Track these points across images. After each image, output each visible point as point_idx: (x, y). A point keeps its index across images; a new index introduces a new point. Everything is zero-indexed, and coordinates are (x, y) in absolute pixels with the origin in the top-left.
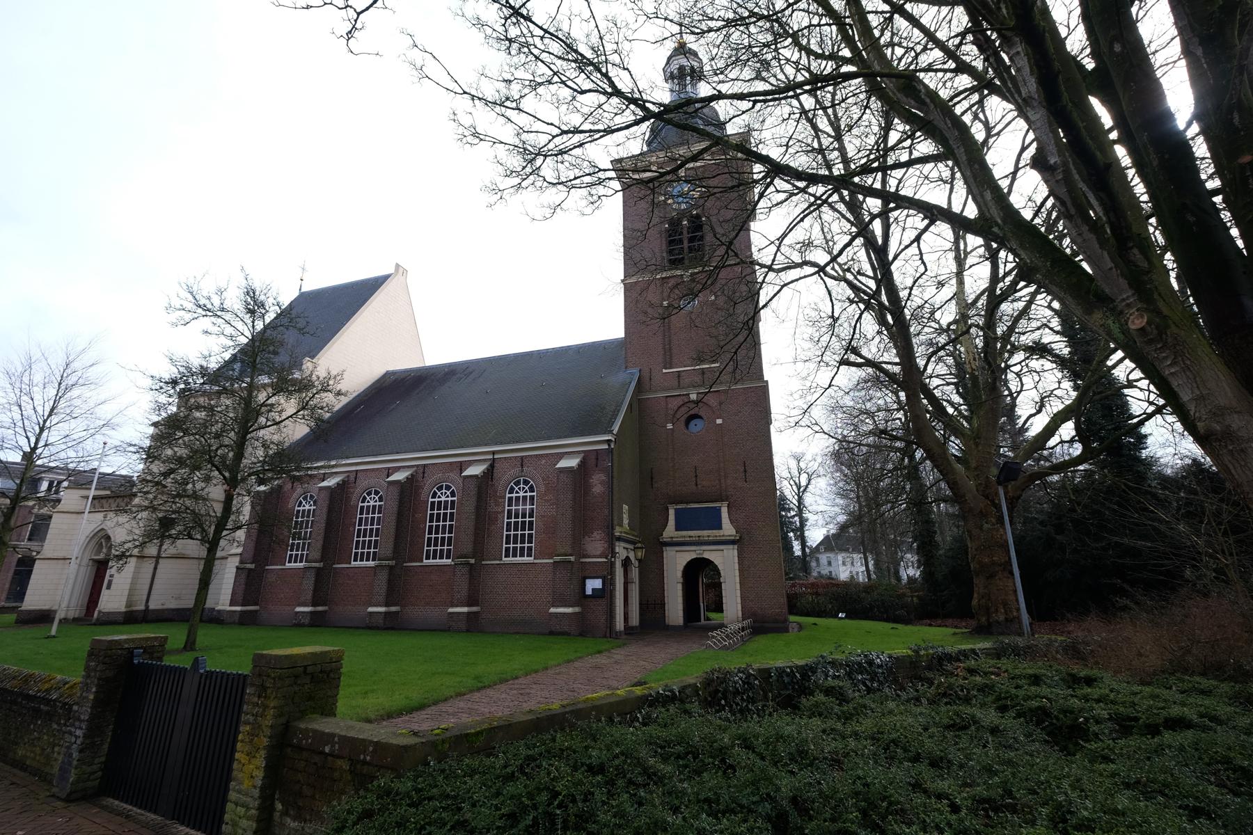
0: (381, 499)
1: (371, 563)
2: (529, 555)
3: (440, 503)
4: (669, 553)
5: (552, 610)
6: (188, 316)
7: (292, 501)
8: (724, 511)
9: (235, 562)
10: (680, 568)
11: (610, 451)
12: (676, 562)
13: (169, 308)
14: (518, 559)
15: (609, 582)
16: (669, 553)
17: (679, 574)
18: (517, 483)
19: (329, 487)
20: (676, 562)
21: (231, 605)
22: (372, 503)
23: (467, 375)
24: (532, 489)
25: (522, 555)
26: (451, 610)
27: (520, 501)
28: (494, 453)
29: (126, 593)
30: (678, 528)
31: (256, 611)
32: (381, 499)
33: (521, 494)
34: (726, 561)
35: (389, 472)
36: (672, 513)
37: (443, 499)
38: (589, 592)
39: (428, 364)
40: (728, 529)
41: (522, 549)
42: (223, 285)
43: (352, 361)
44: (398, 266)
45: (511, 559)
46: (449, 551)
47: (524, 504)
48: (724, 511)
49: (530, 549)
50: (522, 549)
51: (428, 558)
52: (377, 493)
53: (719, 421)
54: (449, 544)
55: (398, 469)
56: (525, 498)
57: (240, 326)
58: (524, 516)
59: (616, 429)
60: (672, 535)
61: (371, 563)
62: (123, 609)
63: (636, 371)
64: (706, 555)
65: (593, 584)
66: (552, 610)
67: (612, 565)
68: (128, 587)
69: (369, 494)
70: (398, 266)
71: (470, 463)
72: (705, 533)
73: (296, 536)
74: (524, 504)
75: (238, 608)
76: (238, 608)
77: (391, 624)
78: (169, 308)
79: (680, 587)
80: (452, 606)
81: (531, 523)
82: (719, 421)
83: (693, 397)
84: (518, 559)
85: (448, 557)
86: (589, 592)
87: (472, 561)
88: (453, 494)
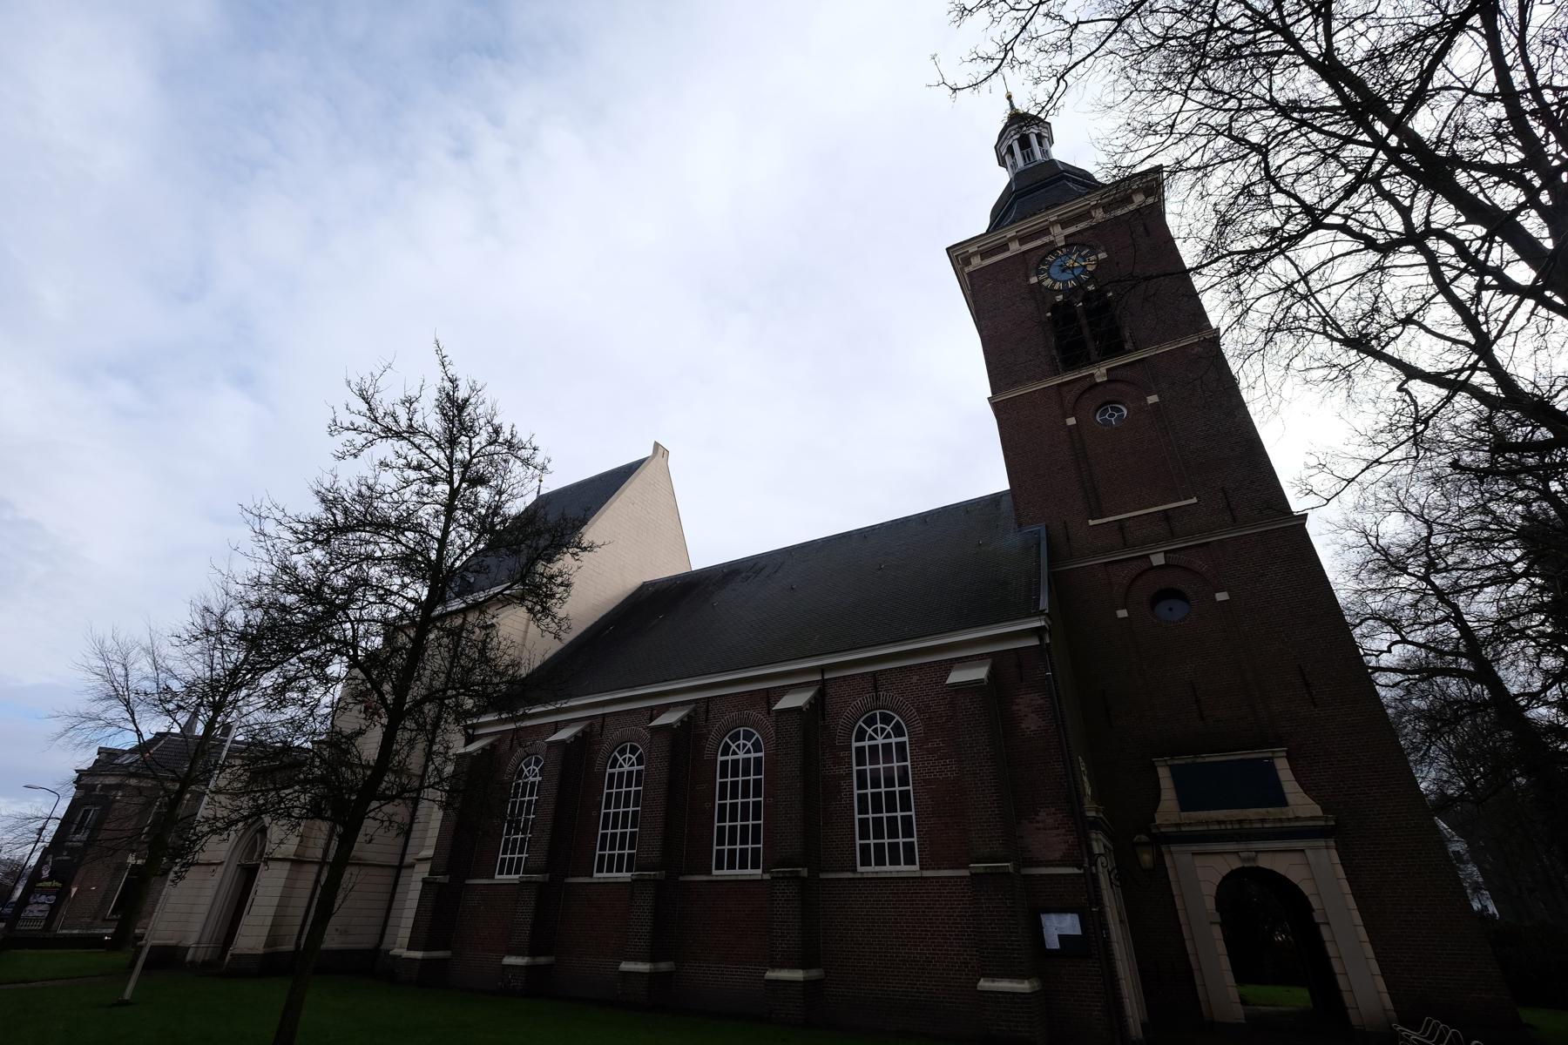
0: (640, 761)
1: (625, 876)
2: (910, 861)
3: (735, 762)
4: (1179, 859)
5: (984, 984)
6: (360, 440)
7: (510, 768)
8: (1283, 767)
9: (423, 871)
10: (1209, 890)
11: (1039, 650)
12: (1200, 876)
13: (335, 428)
14: (888, 869)
15: (1093, 922)
16: (1179, 859)
17: (1210, 904)
18: (871, 721)
19: (562, 742)
20: (1200, 876)
21: (409, 949)
22: (626, 768)
23: (758, 573)
24: (898, 731)
25: (895, 861)
26: (770, 975)
27: (882, 749)
28: (822, 669)
29: (269, 921)
30: (1186, 804)
31: (444, 960)
32: (640, 761)
33: (880, 741)
34: (1316, 872)
35: (655, 712)
36: (1164, 774)
37: (741, 755)
38: (1053, 943)
39: (694, 568)
40: (1301, 804)
41: (894, 847)
42: (414, 393)
43: (601, 574)
44: (657, 445)
45: (872, 869)
46: (756, 851)
47: (888, 759)
48: (1283, 767)
49: (909, 847)
50: (894, 847)
51: (720, 867)
52: (633, 750)
53: (1222, 596)
54: (756, 840)
55: (666, 708)
56: (887, 747)
57: (435, 453)
58: (889, 782)
59: (1044, 604)
60: (1174, 818)
61: (625, 876)
62: (261, 950)
63: (1040, 528)
64: (1264, 862)
65: (1060, 926)
66: (984, 984)
67: (1095, 879)
68: (272, 911)
69: (622, 752)
70: (657, 445)
71: (784, 691)
72: (1251, 813)
73: (515, 826)
74: (888, 759)
75: (418, 955)
76: (418, 955)
77: (660, 1000)
78: (335, 428)
79: (1217, 931)
80: (774, 967)
81: (905, 795)
82: (1222, 596)
83: (1158, 560)
84: (888, 869)
85: (755, 866)
86: (1053, 943)
87: (804, 872)
88: (757, 748)
